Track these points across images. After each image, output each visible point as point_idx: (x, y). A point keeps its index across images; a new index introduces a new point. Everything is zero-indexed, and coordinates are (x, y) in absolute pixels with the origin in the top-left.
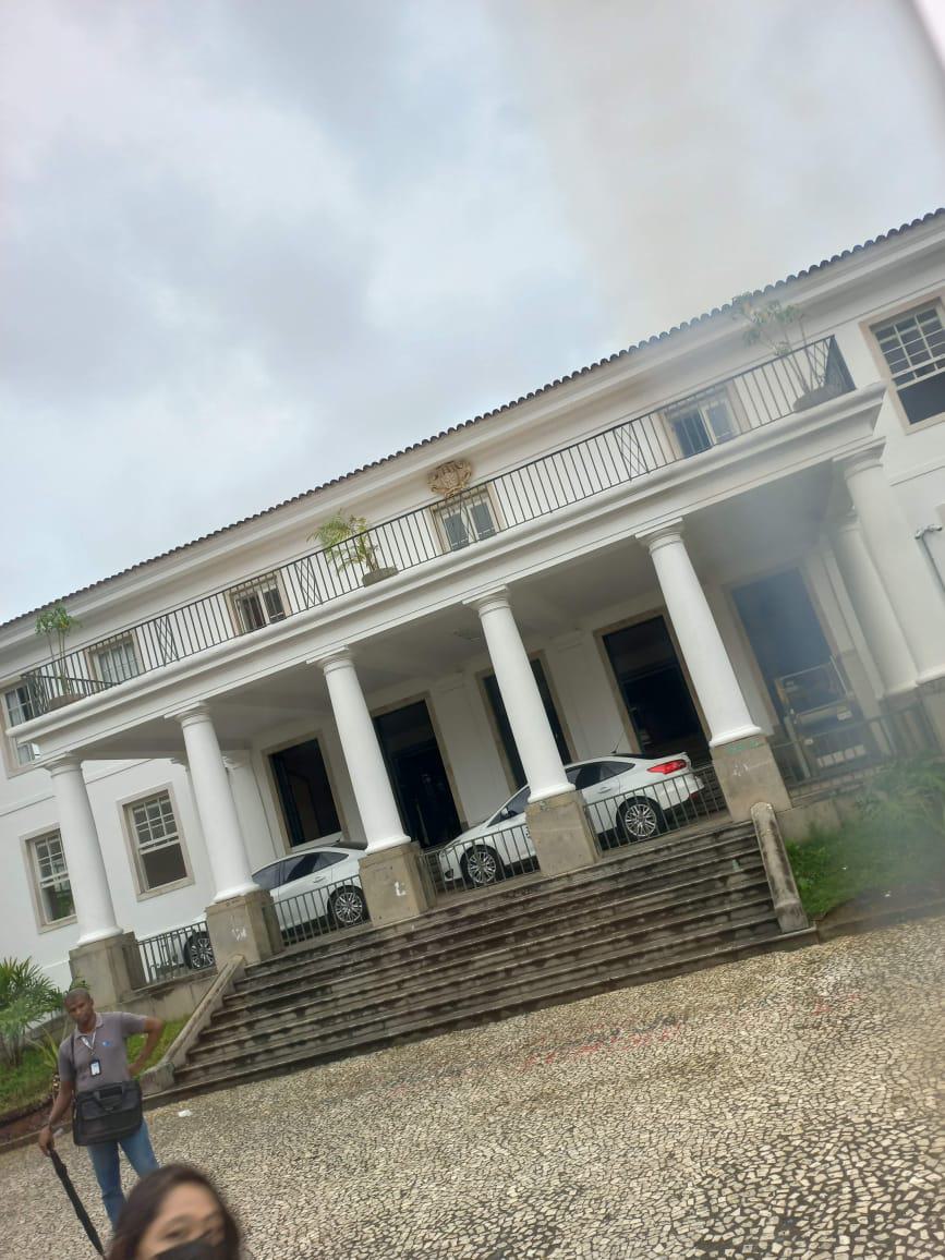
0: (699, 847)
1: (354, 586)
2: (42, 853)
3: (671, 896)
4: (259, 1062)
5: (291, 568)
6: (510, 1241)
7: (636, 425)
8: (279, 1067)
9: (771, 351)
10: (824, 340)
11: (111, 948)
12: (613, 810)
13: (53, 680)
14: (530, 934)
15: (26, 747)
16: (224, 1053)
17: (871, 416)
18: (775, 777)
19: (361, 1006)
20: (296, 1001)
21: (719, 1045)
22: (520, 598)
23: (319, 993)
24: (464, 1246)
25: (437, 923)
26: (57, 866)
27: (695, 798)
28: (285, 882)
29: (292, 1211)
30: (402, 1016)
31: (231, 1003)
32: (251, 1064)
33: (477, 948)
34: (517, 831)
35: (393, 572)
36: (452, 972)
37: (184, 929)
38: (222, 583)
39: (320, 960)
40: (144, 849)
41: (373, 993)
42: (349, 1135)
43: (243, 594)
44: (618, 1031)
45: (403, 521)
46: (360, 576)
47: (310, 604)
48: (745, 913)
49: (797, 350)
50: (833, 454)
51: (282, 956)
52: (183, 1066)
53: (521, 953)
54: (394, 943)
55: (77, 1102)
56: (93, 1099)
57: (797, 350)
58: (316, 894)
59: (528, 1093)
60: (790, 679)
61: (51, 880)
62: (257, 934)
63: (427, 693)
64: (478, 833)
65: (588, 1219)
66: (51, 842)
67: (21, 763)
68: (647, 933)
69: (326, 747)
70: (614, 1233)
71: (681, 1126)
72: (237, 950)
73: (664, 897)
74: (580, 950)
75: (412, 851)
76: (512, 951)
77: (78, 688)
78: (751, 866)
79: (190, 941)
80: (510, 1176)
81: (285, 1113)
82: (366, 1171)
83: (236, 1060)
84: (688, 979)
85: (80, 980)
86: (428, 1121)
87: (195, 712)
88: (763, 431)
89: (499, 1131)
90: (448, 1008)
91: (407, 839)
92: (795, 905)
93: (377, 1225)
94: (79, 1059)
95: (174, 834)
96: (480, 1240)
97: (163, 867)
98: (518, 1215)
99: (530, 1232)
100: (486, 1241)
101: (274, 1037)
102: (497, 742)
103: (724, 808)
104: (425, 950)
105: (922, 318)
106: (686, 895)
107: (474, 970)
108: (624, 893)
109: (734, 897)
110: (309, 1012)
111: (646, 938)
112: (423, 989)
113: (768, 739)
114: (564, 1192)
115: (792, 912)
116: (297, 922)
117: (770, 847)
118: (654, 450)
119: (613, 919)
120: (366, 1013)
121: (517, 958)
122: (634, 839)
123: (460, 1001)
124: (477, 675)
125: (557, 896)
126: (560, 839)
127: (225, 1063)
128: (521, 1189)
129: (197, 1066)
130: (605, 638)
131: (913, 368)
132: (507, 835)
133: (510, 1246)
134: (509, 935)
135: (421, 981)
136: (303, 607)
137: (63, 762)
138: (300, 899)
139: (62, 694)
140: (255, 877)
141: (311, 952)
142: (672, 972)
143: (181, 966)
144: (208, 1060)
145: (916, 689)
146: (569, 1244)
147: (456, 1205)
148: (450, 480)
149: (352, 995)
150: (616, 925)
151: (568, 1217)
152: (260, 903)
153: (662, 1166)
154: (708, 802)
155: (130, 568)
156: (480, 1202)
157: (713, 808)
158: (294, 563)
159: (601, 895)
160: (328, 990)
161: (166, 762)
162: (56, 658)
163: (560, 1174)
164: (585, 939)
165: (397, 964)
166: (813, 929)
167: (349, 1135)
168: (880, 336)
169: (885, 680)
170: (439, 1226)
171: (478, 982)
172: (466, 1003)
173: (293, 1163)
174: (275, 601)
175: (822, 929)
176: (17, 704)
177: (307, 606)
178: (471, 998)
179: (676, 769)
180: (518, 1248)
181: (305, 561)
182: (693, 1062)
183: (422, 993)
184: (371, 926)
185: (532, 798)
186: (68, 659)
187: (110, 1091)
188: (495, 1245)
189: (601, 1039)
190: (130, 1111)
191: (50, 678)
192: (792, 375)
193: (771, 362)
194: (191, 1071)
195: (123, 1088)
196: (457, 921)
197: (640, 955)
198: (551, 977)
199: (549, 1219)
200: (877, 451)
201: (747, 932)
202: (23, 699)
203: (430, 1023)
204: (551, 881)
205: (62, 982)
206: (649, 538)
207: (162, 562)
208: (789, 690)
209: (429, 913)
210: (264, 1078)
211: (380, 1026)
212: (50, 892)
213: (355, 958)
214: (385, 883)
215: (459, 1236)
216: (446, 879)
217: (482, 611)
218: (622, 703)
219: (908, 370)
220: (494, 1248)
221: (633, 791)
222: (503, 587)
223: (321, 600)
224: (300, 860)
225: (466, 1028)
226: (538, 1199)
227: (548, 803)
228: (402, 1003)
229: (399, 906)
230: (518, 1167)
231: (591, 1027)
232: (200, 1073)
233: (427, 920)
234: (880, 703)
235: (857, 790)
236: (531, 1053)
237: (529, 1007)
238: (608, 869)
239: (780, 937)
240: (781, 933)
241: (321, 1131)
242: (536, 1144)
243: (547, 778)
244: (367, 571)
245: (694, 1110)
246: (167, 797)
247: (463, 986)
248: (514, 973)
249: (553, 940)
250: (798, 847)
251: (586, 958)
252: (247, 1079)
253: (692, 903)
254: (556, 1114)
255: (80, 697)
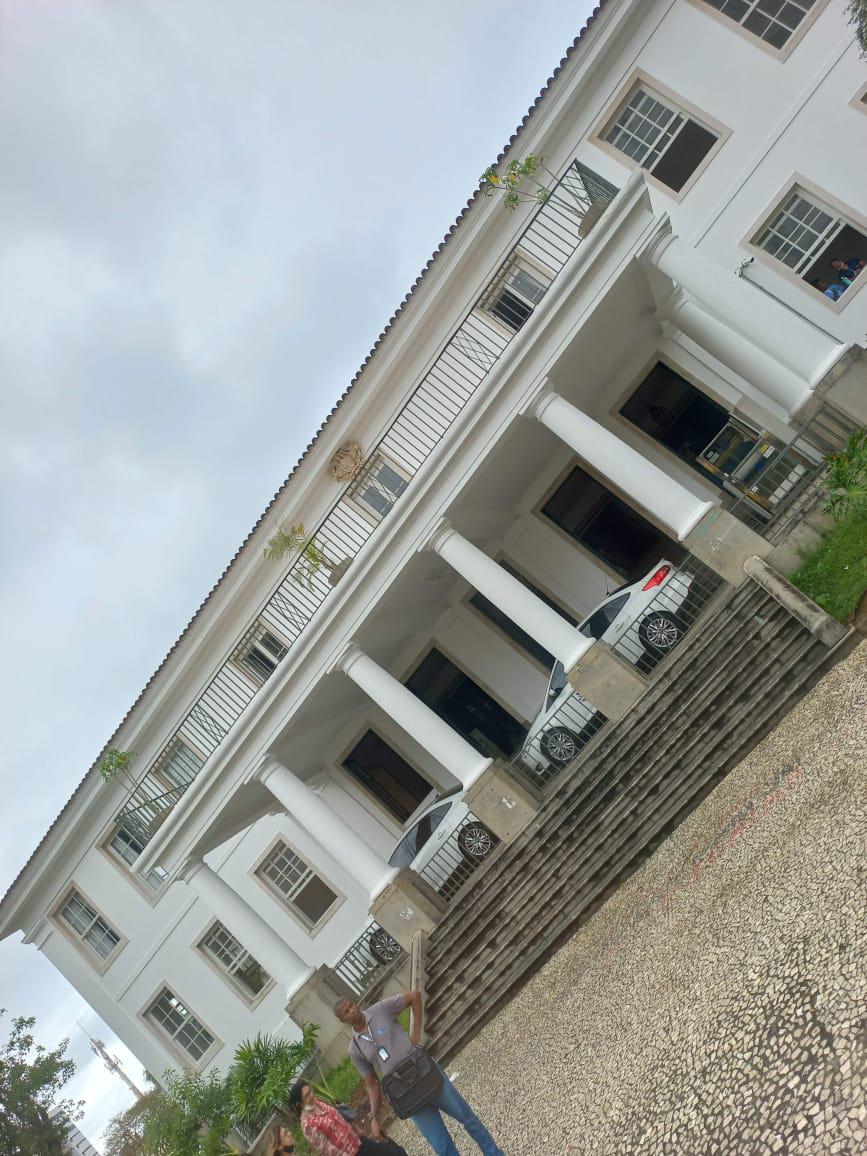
0: (721, 624)
1: (326, 591)
2: (215, 948)
3: (724, 675)
4: (485, 1003)
5: (269, 607)
6: (776, 1013)
7: (466, 327)
8: (504, 995)
9: (534, 203)
10: (570, 168)
11: (314, 987)
12: (635, 637)
13: (141, 809)
14: (632, 773)
15: (152, 874)
16: (454, 1012)
17: (644, 203)
18: (748, 533)
19: (536, 910)
20: (483, 939)
21: (838, 763)
22: (458, 519)
23: (497, 921)
24: (742, 1039)
25: (554, 810)
26: (232, 952)
27: (693, 588)
28: (416, 854)
29: (588, 1097)
30: (574, 898)
31: (435, 970)
32: (481, 1007)
33: (599, 810)
34: (571, 701)
35: (349, 561)
36: (590, 841)
37: (362, 936)
38: (265, 593)
39: (482, 895)
40: (291, 896)
41: (540, 895)
42: (594, 1013)
43: (245, 651)
44: (751, 803)
45: (332, 517)
46: (326, 581)
47: (302, 627)
48: (790, 652)
49: (555, 189)
50: (241, 780)
51: (451, 910)
52: (428, 1043)
53: (635, 792)
54: (531, 847)
55: (386, 1086)
56: (395, 1079)
57: (555, 189)
58: (446, 846)
59: (713, 894)
60: (707, 452)
61: (235, 965)
62: (421, 906)
63: (433, 640)
64: (541, 722)
65: (827, 959)
66: (217, 935)
67: (156, 889)
68: (723, 716)
69: (384, 733)
70: (855, 956)
71: (852, 843)
72: (413, 928)
73: (719, 679)
74: (680, 761)
75: (499, 768)
76: (627, 795)
77: (163, 803)
78: (773, 612)
79: (372, 943)
80: (742, 965)
81: (532, 1028)
82: (626, 1031)
83: (467, 1012)
84: (779, 730)
85: (307, 1026)
86: (649, 963)
87: (265, 764)
88: (568, 268)
89: (710, 937)
90: (605, 869)
91: (489, 761)
92: (826, 621)
93: (663, 1066)
94: (368, 1053)
95: (307, 871)
96: (752, 1026)
97: (315, 901)
98: (769, 990)
99: (788, 997)
100: (758, 1025)
101: (484, 976)
102: (510, 644)
103: (721, 581)
104: (559, 837)
105: (634, 104)
106: (735, 667)
107: (606, 828)
108: (685, 697)
109: (773, 644)
110: (499, 940)
111: (725, 721)
112: (577, 867)
113: (721, 506)
114: (793, 950)
115: (828, 627)
116: (446, 877)
117: (778, 589)
118: (493, 337)
119: (690, 722)
120: (544, 913)
121: (633, 798)
122: (666, 650)
123: (612, 858)
124: (462, 602)
125: (634, 732)
126: (609, 686)
127: (459, 1020)
128: (758, 968)
129: (440, 1035)
130: (544, 511)
131: (651, 148)
132: (565, 708)
133: (780, 1017)
134: (617, 785)
135: (571, 862)
136: (297, 632)
137: (188, 866)
138: (432, 864)
139: (154, 816)
140: (391, 863)
141: (471, 893)
142: (763, 732)
143: (378, 966)
144: (444, 1026)
145: (814, 394)
146: (825, 986)
147: (715, 1012)
148: (347, 464)
149: (524, 907)
150: (695, 724)
151: (810, 967)
152: (408, 881)
153: (858, 881)
154: (705, 585)
155: (195, 615)
156: (732, 998)
157: (699, 602)
158: (269, 602)
159: (668, 709)
160: (503, 914)
161: (267, 818)
162: (133, 791)
163: (781, 939)
164: (677, 751)
165: (544, 861)
166: (853, 629)
167: (594, 1013)
168: (610, 139)
169: (783, 404)
170: (713, 1037)
171: (616, 836)
172: (617, 857)
173: (564, 1060)
174: (272, 642)
175: (860, 625)
176: (124, 846)
177: (299, 629)
178: (618, 851)
179: (664, 577)
180: (787, 1014)
181: (276, 596)
182: (827, 789)
183: (577, 871)
184: (505, 845)
185: (567, 669)
186: (143, 785)
187: (404, 1068)
188: (767, 1024)
189: (742, 818)
190: (427, 1075)
191: (138, 809)
192: (567, 214)
193: (540, 211)
194: (436, 1044)
195: (414, 1060)
196: (568, 800)
197: (729, 735)
198: (670, 796)
199: (796, 977)
200: (666, 227)
201: (801, 666)
202: (126, 839)
203: (599, 890)
204: (622, 722)
205: (296, 1036)
206: (531, 409)
207: (166, 667)
208: (713, 460)
209: (543, 807)
210: (496, 1013)
211: (561, 916)
212: (239, 973)
213: (508, 876)
214: (495, 805)
215: (733, 1035)
216: (540, 773)
217: (437, 548)
218: (588, 552)
219: (649, 152)
220: (768, 1026)
221: (643, 613)
222: (442, 520)
223: (225, 731)
224: (415, 832)
225: (630, 876)
226: (776, 968)
227: (582, 664)
228: (567, 888)
229: (516, 817)
230: (743, 955)
231: (728, 814)
232: (446, 1038)
233: (545, 814)
234: (790, 424)
235: (817, 501)
236: (694, 862)
237: (668, 829)
238: (661, 686)
239: (830, 652)
240: (829, 649)
241: (569, 1023)
242: (745, 927)
243: (569, 646)
244: (328, 573)
245: (854, 825)
246: (284, 845)
247: (607, 845)
248: (639, 812)
249: (653, 766)
250: (799, 575)
251: (688, 765)
252: (485, 1020)
253: (745, 670)
254: (746, 895)
255: (170, 809)
